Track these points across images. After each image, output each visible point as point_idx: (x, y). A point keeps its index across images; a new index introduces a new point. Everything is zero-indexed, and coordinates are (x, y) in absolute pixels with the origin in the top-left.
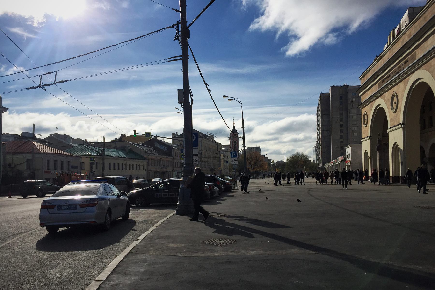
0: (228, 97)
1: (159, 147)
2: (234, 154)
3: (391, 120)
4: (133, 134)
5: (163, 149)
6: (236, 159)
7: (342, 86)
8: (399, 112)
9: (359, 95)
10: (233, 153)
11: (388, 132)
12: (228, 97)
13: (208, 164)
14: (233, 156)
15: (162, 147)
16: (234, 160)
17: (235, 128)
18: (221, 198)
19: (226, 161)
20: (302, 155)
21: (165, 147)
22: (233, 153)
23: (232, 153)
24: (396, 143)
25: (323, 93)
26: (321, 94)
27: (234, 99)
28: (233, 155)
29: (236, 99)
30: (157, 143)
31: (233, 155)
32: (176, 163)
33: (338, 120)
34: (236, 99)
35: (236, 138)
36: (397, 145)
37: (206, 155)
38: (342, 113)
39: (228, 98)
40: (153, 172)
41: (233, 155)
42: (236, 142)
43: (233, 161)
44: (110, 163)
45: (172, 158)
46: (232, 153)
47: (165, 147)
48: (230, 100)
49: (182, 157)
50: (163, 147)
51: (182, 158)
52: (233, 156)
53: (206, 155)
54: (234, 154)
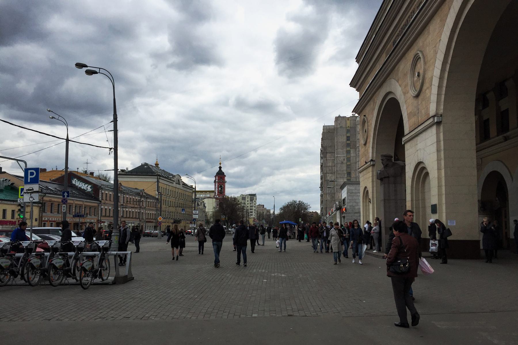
0: (86, 66)
1: (80, 186)
2: (32, 174)
3: (410, 115)
4: (56, 170)
5: (85, 188)
6: (36, 187)
7: (349, 117)
8: (427, 91)
9: (448, 221)
10: (31, 173)
11: (403, 143)
12: (86, 66)
13: (170, 213)
14: (29, 181)
15: (84, 186)
16: (31, 190)
17: (222, 169)
18: (242, 253)
19: (183, 209)
20: (299, 204)
21: (88, 186)
22: (31, 173)
23: (29, 171)
24: (419, 163)
25: (326, 125)
26: (324, 126)
27: (97, 70)
28: (30, 178)
29: (101, 71)
30: (76, 179)
31: (29, 177)
32: (149, 215)
33: (344, 159)
34: (101, 71)
35: (222, 181)
36: (424, 168)
37: (176, 203)
38: (350, 151)
39: (85, 69)
40: (54, 223)
41: (30, 178)
42: (223, 186)
43: (28, 193)
45: (99, 202)
46: (29, 171)
47: (88, 186)
48: (90, 73)
49: (21, 193)
50: (86, 185)
51: (21, 196)
52: (29, 181)
53: (176, 203)
54: (32, 174)
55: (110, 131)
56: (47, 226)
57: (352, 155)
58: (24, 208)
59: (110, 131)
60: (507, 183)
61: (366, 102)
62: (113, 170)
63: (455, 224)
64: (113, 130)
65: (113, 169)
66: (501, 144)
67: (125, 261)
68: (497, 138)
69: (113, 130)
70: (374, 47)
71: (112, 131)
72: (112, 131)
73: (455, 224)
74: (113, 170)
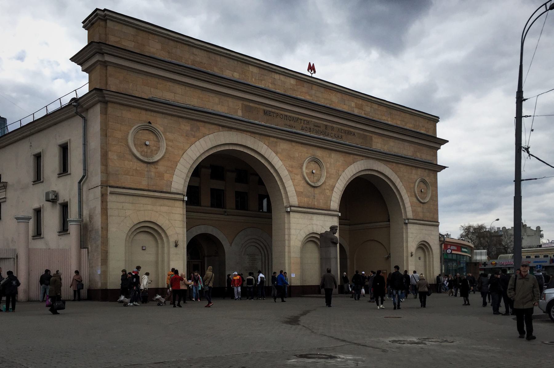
41: (99, 17)
44: (448, 167)
55: (527, 116)
56: (188, 206)
57: (510, 255)
58: (165, 305)
59: (527, 116)
60: (225, 247)
61: (161, 110)
62: (523, 180)
63: (294, 276)
64: (523, 117)
65: (522, 182)
66: (197, 213)
67: (536, 256)
68: (210, 208)
69: (523, 117)
70: (253, 91)
71: (525, 117)
72: (525, 117)
73: (294, 276)
74: (523, 180)
